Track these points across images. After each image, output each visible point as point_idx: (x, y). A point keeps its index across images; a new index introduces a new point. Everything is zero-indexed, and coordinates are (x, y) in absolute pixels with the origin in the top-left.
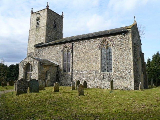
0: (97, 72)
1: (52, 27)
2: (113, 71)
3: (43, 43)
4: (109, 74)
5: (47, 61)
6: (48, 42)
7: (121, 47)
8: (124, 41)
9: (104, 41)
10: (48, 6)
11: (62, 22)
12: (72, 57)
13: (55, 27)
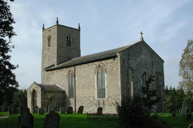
1: (65, 44)
2: (106, 98)
3: (54, 65)
5: (54, 87)
6: (59, 64)
7: (112, 72)
9: (99, 66)
10: (57, 22)
11: (79, 36)
12: (75, 82)
13: (69, 43)
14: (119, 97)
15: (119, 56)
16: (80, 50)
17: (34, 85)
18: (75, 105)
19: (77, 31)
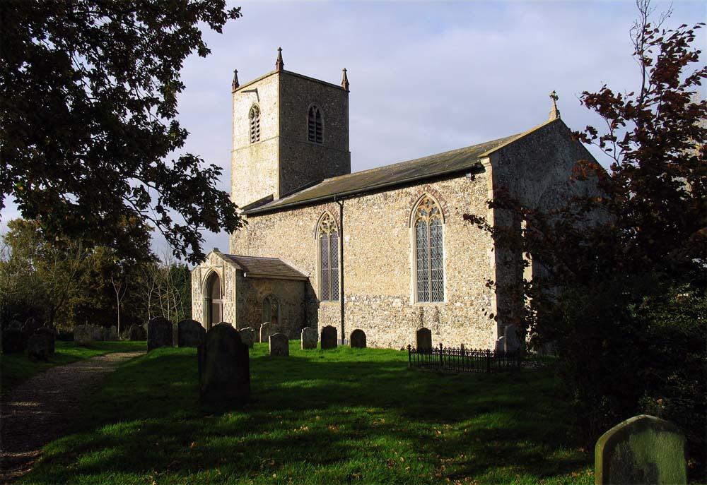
0: (405, 303)
3: (270, 199)
4: (436, 307)
5: (276, 263)
6: (286, 196)
8: (473, 198)
13: (315, 132)
14: (489, 297)
15: (489, 169)
16: (347, 154)
17: (214, 259)
18: (343, 321)
19: (339, 93)
